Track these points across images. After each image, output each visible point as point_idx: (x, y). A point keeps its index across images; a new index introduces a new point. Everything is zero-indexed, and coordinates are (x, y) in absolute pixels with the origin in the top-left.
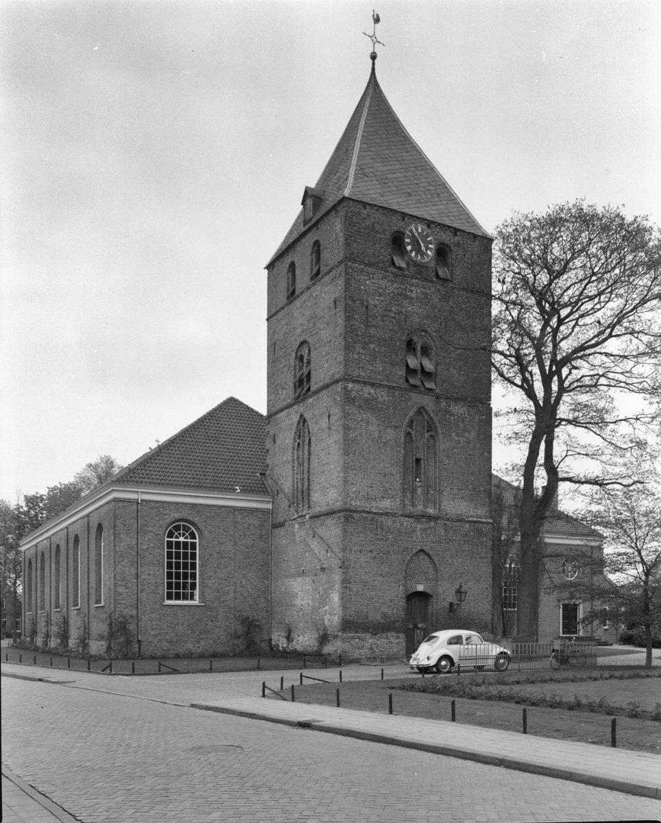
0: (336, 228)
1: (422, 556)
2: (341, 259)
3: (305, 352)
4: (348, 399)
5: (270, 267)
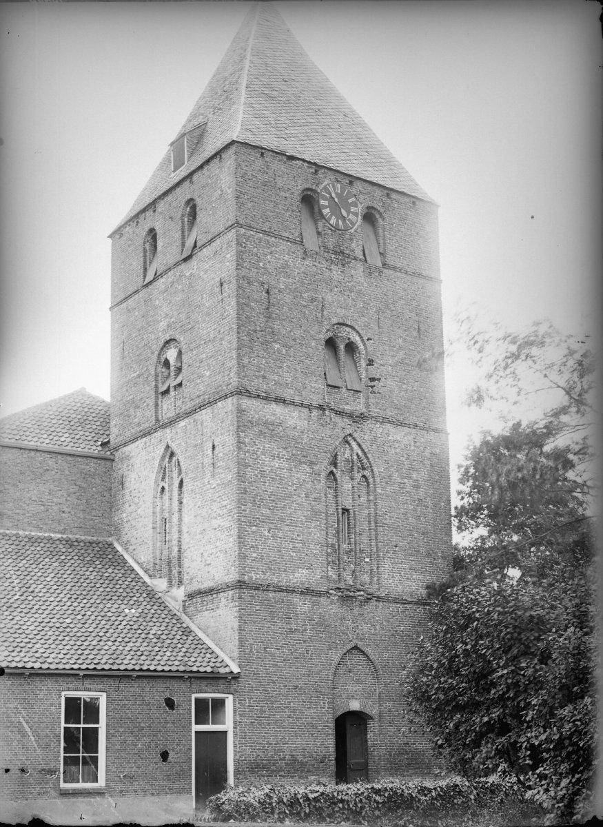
0: (224, 176)
1: (356, 658)
2: (230, 223)
3: (171, 354)
4: (243, 423)
5: (172, 144)
